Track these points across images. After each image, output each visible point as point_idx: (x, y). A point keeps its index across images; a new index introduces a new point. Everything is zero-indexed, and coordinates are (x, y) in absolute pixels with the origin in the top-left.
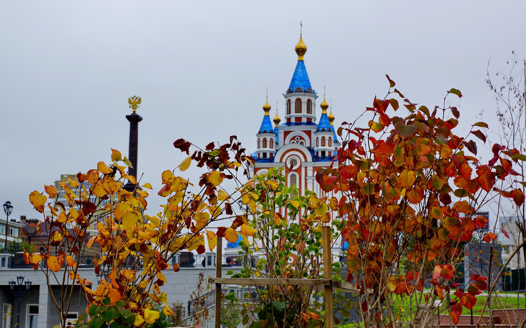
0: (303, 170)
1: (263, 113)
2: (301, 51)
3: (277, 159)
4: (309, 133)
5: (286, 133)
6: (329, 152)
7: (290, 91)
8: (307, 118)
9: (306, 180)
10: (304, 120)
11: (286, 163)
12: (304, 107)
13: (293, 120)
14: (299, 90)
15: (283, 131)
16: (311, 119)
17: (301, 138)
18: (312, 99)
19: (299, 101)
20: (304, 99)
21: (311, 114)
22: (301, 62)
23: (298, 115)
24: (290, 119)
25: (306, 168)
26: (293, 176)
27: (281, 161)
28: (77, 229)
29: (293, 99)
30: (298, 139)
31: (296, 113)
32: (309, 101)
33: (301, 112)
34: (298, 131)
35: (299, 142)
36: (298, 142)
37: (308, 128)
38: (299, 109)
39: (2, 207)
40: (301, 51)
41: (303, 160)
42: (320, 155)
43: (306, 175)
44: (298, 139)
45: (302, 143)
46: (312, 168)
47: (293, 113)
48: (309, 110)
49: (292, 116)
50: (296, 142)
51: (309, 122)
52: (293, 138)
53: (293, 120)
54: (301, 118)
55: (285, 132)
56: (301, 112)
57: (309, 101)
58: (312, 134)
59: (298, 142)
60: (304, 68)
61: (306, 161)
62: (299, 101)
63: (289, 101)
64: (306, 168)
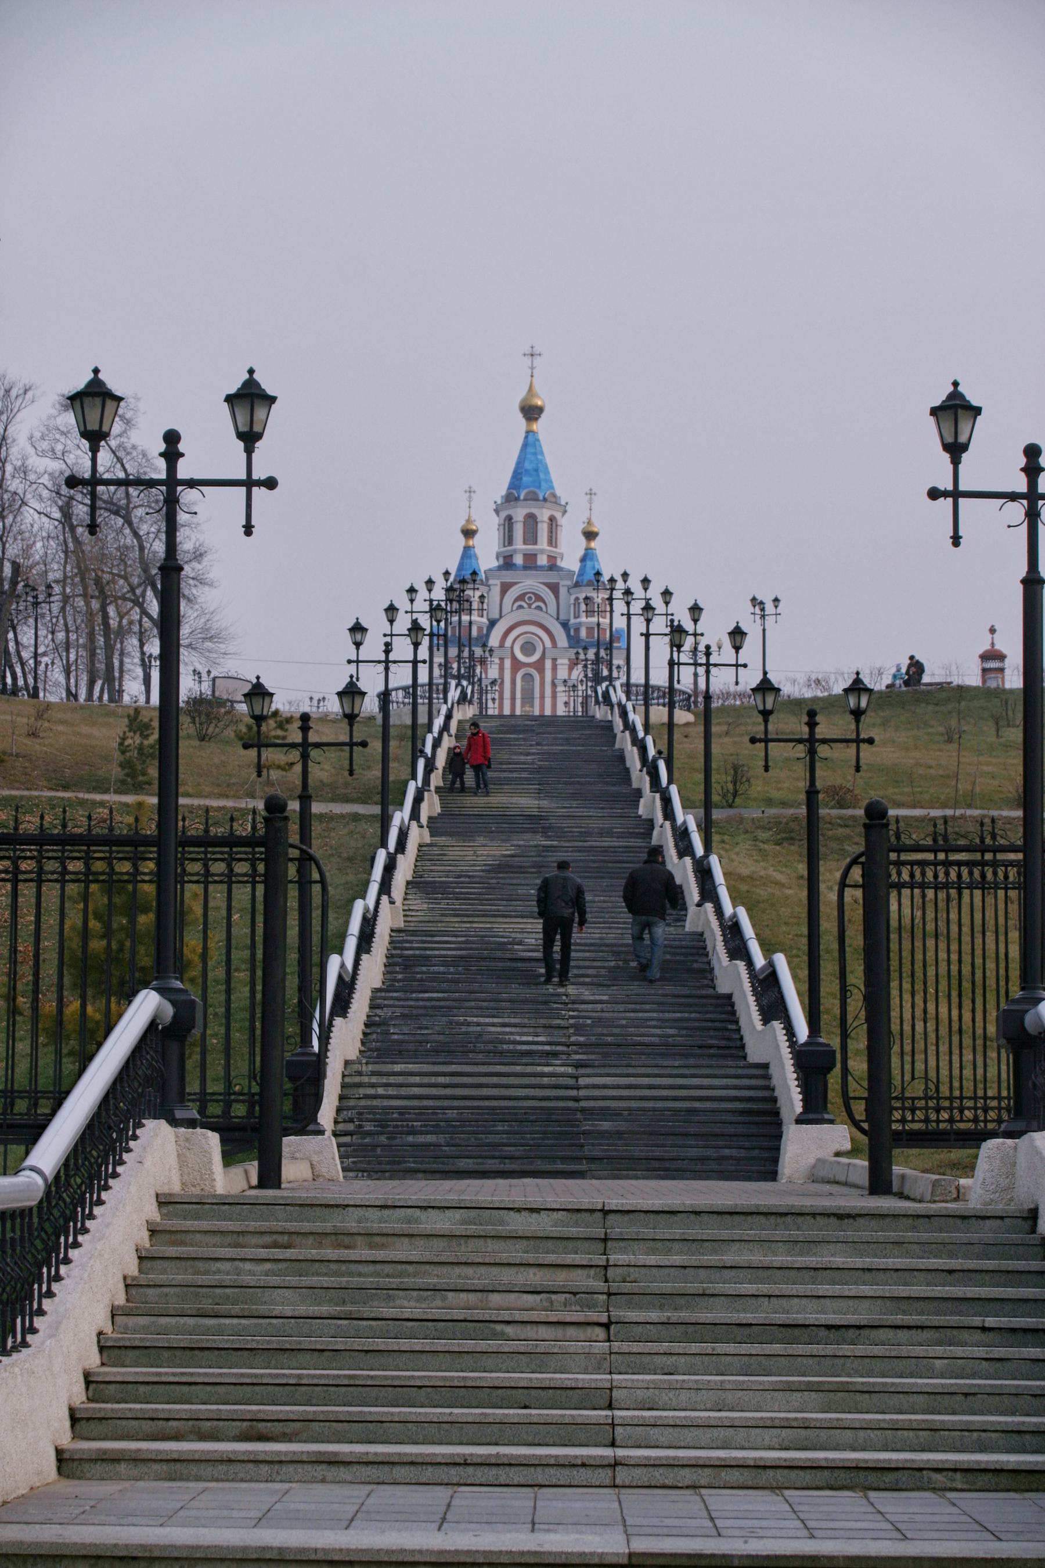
0: (548, 664)
1: (461, 540)
2: (531, 412)
4: (554, 588)
5: (505, 588)
6: (587, 628)
7: (510, 498)
8: (549, 556)
9: (554, 685)
10: (542, 561)
11: (512, 648)
12: (543, 530)
13: (519, 560)
14: (533, 497)
15: (498, 582)
16: (555, 558)
17: (539, 598)
18: (558, 515)
19: (531, 519)
20: (544, 514)
21: (556, 547)
22: (530, 444)
24: (511, 556)
25: (554, 660)
26: (528, 678)
28: (370, 705)
29: (519, 514)
30: (530, 598)
31: (525, 543)
32: (552, 519)
33: (535, 543)
34: (530, 583)
35: (534, 606)
36: (530, 605)
37: (552, 577)
38: (531, 536)
39: (384, 613)
40: (531, 412)
41: (548, 644)
44: (530, 598)
45: (539, 608)
46: (566, 661)
47: (519, 545)
48: (552, 541)
49: (515, 551)
50: (525, 605)
51: (553, 567)
52: (521, 597)
53: (519, 560)
54: (535, 555)
55: (502, 584)
56: (535, 543)
57: (552, 519)
58: (563, 591)
59: (530, 605)
60: (538, 452)
62: (531, 519)
63: (509, 518)
64: (554, 660)
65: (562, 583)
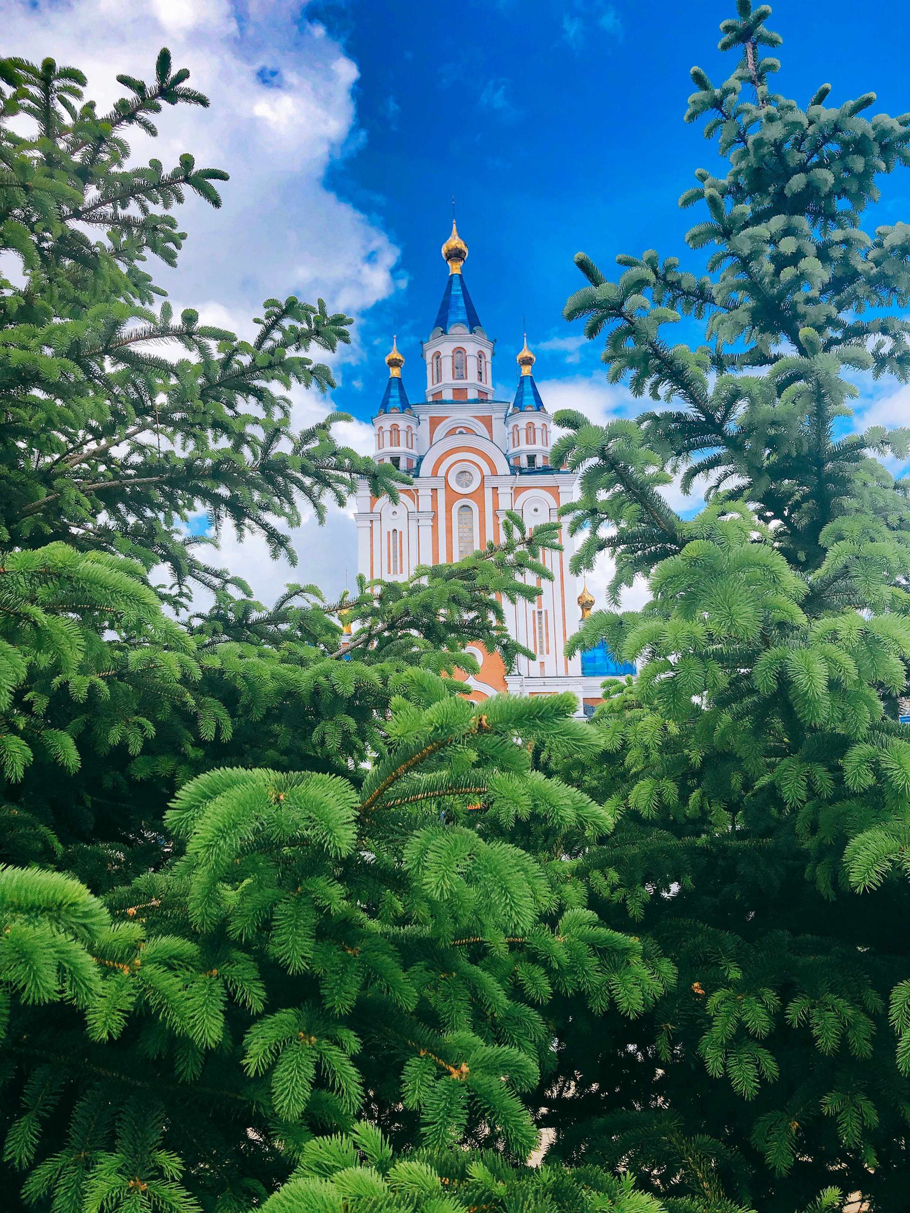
0: (488, 493)
3: (426, 469)
4: (487, 422)
5: (435, 422)
10: (472, 394)
13: (448, 395)
23: (460, 383)
27: (435, 474)
37: (482, 410)
41: (487, 470)
42: (524, 462)
43: (435, 528)
52: (451, 432)
61: (494, 474)
65: (494, 416)
